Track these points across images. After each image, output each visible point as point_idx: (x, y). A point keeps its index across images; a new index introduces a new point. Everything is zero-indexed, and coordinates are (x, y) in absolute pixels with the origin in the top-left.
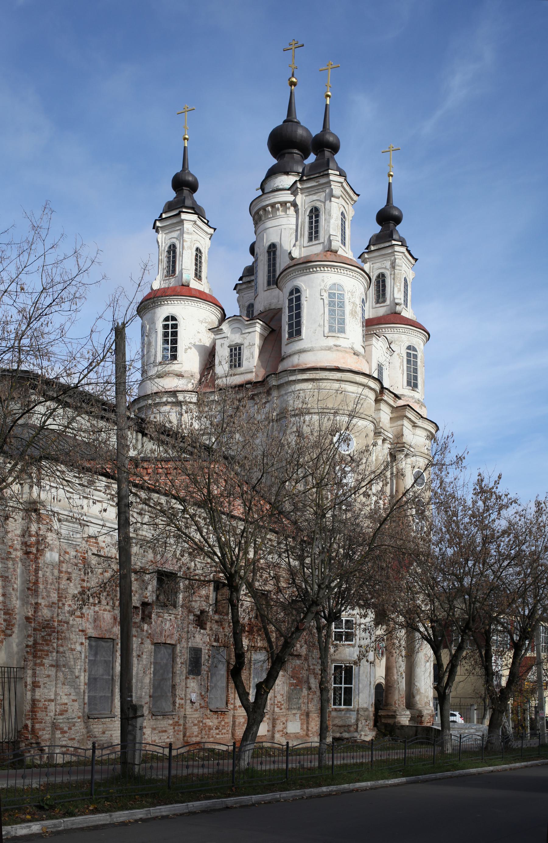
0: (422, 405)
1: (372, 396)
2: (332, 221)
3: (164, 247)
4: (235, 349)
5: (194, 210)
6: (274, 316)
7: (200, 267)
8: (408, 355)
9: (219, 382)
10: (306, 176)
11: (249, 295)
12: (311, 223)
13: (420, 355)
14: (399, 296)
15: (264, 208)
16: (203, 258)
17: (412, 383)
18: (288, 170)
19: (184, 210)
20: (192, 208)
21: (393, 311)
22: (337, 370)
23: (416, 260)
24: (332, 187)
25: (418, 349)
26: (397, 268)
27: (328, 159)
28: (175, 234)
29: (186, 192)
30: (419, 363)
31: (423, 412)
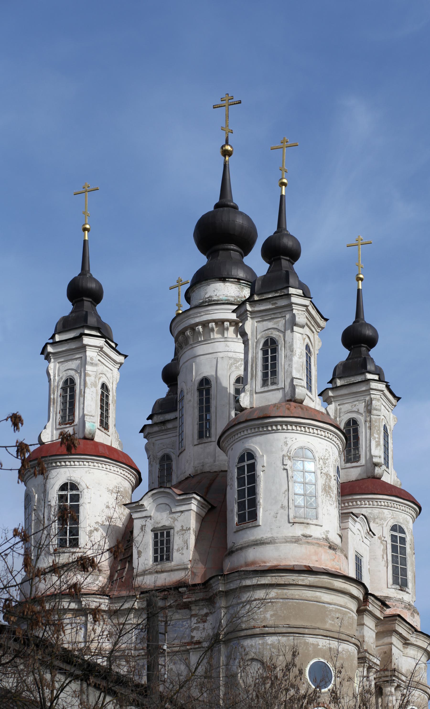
0: (414, 611)
1: (353, 606)
2: (295, 359)
3: (58, 380)
4: (162, 534)
5: (100, 332)
6: (210, 485)
7: (107, 410)
8: (394, 538)
9: (138, 581)
10: (258, 295)
11: (165, 442)
12: (265, 360)
13: (408, 539)
14: (377, 452)
15: (192, 328)
16: (110, 398)
17: (400, 580)
18: (225, 274)
19: (87, 332)
20: (97, 329)
21: (370, 475)
22: (309, 571)
23: (398, 399)
24: (294, 311)
25: (406, 530)
26: (374, 412)
27: (287, 272)
28: (74, 364)
29: (87, 304)
30: (408, 550)
31: (416, 621)
